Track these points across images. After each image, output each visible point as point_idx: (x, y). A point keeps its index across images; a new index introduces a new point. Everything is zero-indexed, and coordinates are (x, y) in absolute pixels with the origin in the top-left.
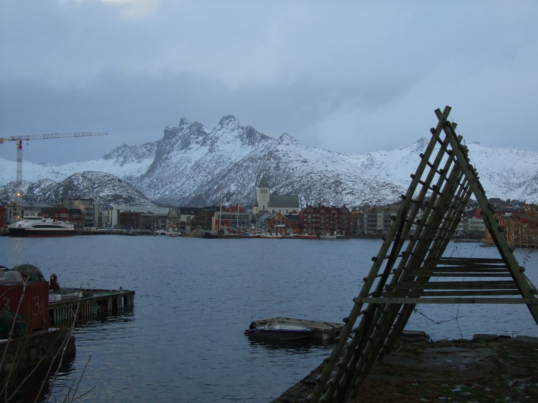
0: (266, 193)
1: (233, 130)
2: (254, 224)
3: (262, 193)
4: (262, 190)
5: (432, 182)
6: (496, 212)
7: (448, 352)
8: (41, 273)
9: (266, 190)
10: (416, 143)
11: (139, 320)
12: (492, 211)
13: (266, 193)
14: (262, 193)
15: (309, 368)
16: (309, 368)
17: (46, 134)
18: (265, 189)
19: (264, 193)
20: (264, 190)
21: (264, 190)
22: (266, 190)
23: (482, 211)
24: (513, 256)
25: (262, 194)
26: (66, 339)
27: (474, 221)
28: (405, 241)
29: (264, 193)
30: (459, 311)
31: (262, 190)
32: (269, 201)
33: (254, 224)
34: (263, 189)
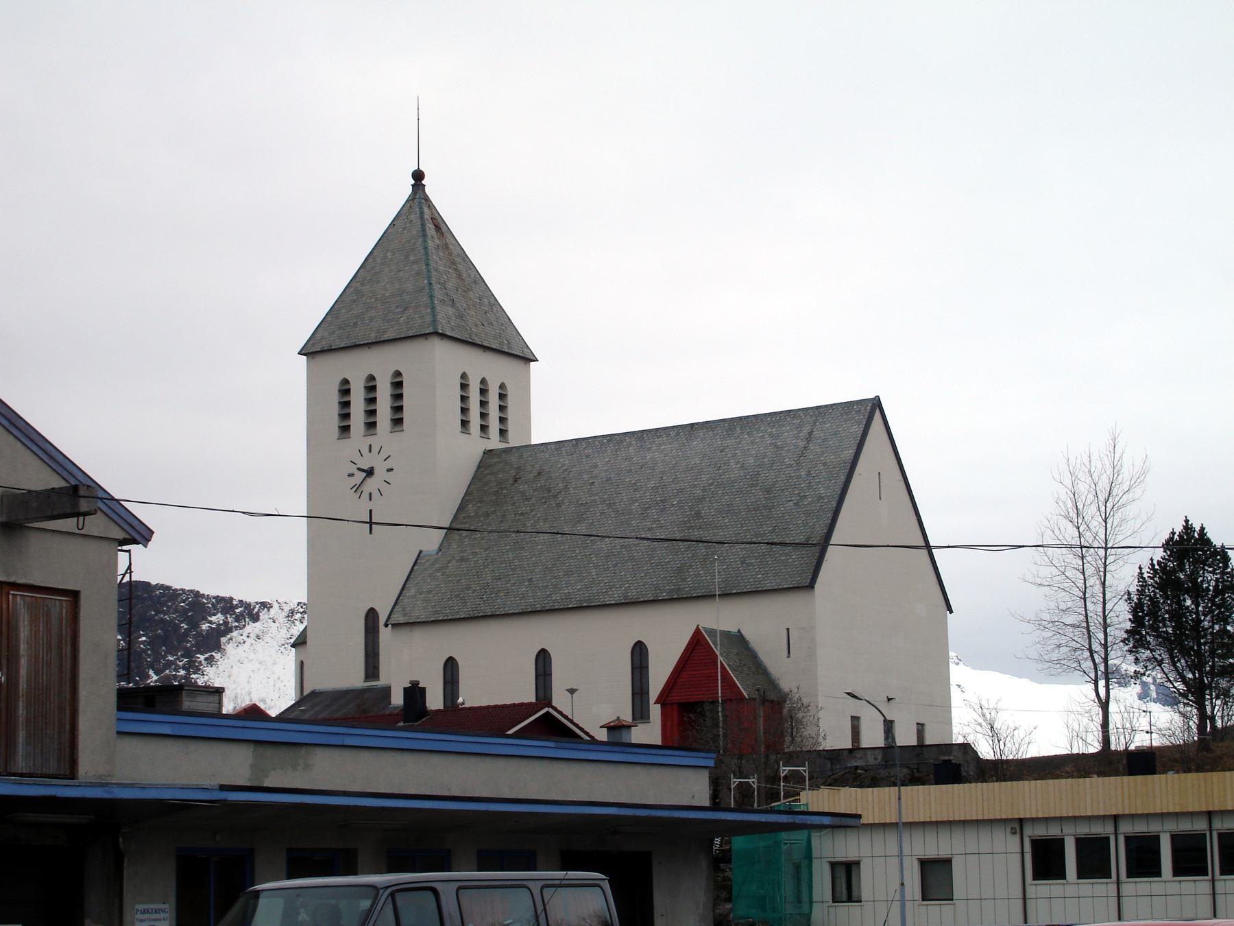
0: (397, 422)
3: (345, 430)
4: (345, 391)
18: (381, 364)
31: (345, 391)
34: (356, 367)
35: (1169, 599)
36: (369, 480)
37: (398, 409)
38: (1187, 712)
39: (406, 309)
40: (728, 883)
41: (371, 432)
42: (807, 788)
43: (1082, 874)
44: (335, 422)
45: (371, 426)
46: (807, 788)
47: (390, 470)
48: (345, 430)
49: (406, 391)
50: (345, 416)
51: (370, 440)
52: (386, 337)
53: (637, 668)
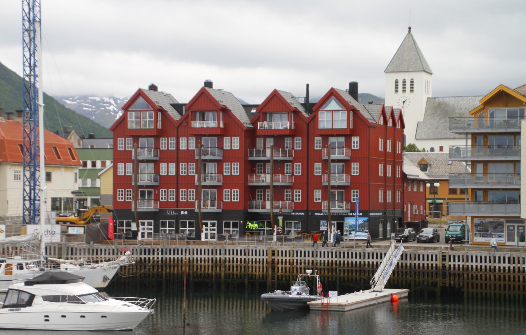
0: (412, 91)
3: (396, 91)
4: (397, 82)
6: (324, 120)
7: (46, 215)
8: (83, 115)
9: (412, 82)
10: (96, 288)
12: (332, 136)
13: (412, 91)
18: (408, 77)
20: (404, 82)
21: (404, 82)
22: (412, 82)
23: (157, 90)
25: (397, 95)
26: (198, 163)
27: (436, 252)
31: (397, 82)
32: (421, 120)
34: (400, 77)
35: (417, 238)
36: (405, 104)
37: (412, 88)
38: (131, 148)
39: (414, 63)
40: (293, 284)
41: (396, 92)
42: (254, 208)
43: (131, 227)
44: (394, 90)
45: (404, 91)
46: (254, 208)
47: (398, 102)
48: (396, 91)
49: (415, 83)
50: (397, 88)
51: (404, 94)
52: (410, 70)
53: (434, 197)
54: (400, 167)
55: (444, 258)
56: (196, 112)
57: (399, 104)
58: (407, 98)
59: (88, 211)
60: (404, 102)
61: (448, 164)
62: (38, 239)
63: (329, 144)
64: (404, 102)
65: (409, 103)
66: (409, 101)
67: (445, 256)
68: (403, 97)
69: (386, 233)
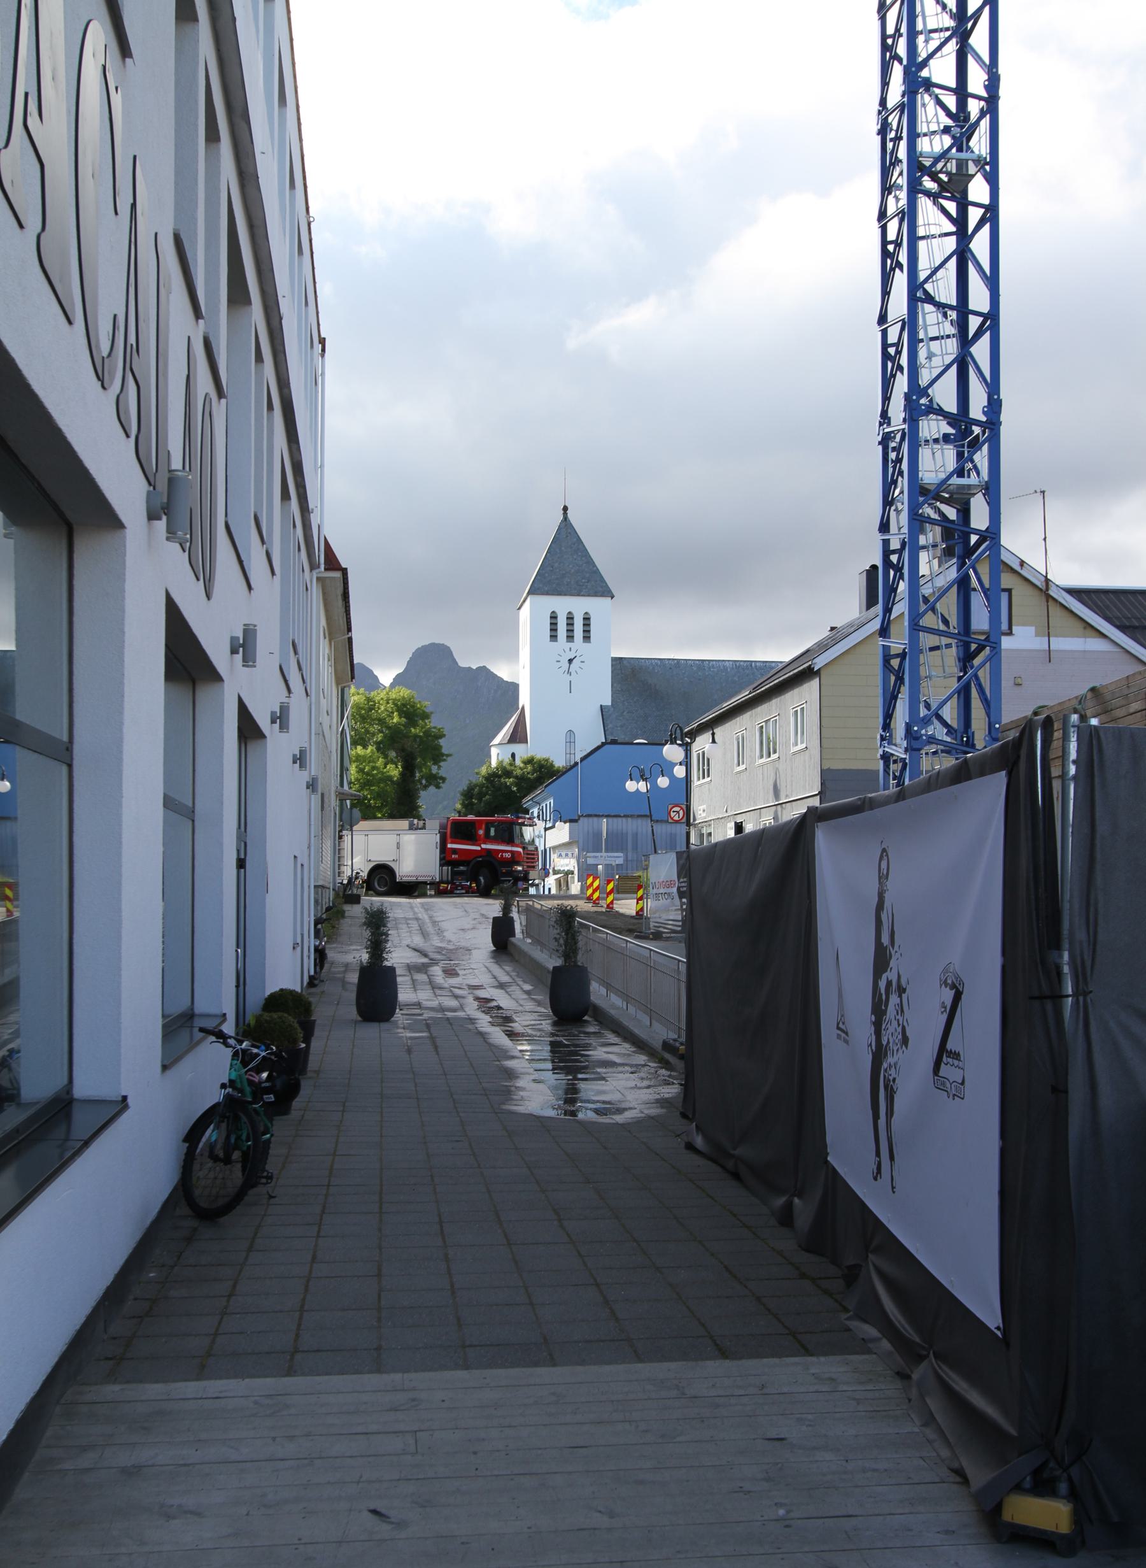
0: (587, 638)
1: (642, 1079)
2: (502, 855)
3: (554, 637)
4: (554, 617)
5: (906, 142)
9: (587, 620)
11: (760, 848)
13: (587, 638)
14: (554, 637)
15: (888, 1042)
16: (888, 1042)
17: (1033, 493)
18: (578, 605)
19: (570, 637)
20: (570, 618)
21: (570, 618)
22: (587, 620)
24: (955, 225)
28: (937, 156)
29: (570, 637)
30: (782, 807)
31: (554, 617)
32: (608, 702)
33: (502, 855)
34: (563, 605)
44: (548, 633)
51: (570, 644)
54: (679, 929)
55: (347, 865)
56: (591, 875)
57: (559, 664)
58: (578, 654)
59: (790, 813)
60: (570, 661)
61: (627, 1009)
62: (235, 1070)
63: (471, 817)
64: (570, 661)
65: (582, 665)
66: (582, 659)
67: (994, 425)
68: (567, 650)
69: (296, 934)
